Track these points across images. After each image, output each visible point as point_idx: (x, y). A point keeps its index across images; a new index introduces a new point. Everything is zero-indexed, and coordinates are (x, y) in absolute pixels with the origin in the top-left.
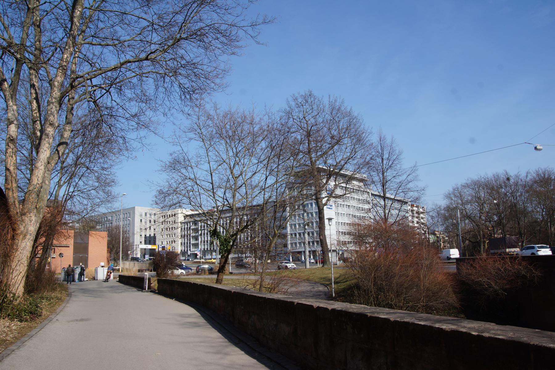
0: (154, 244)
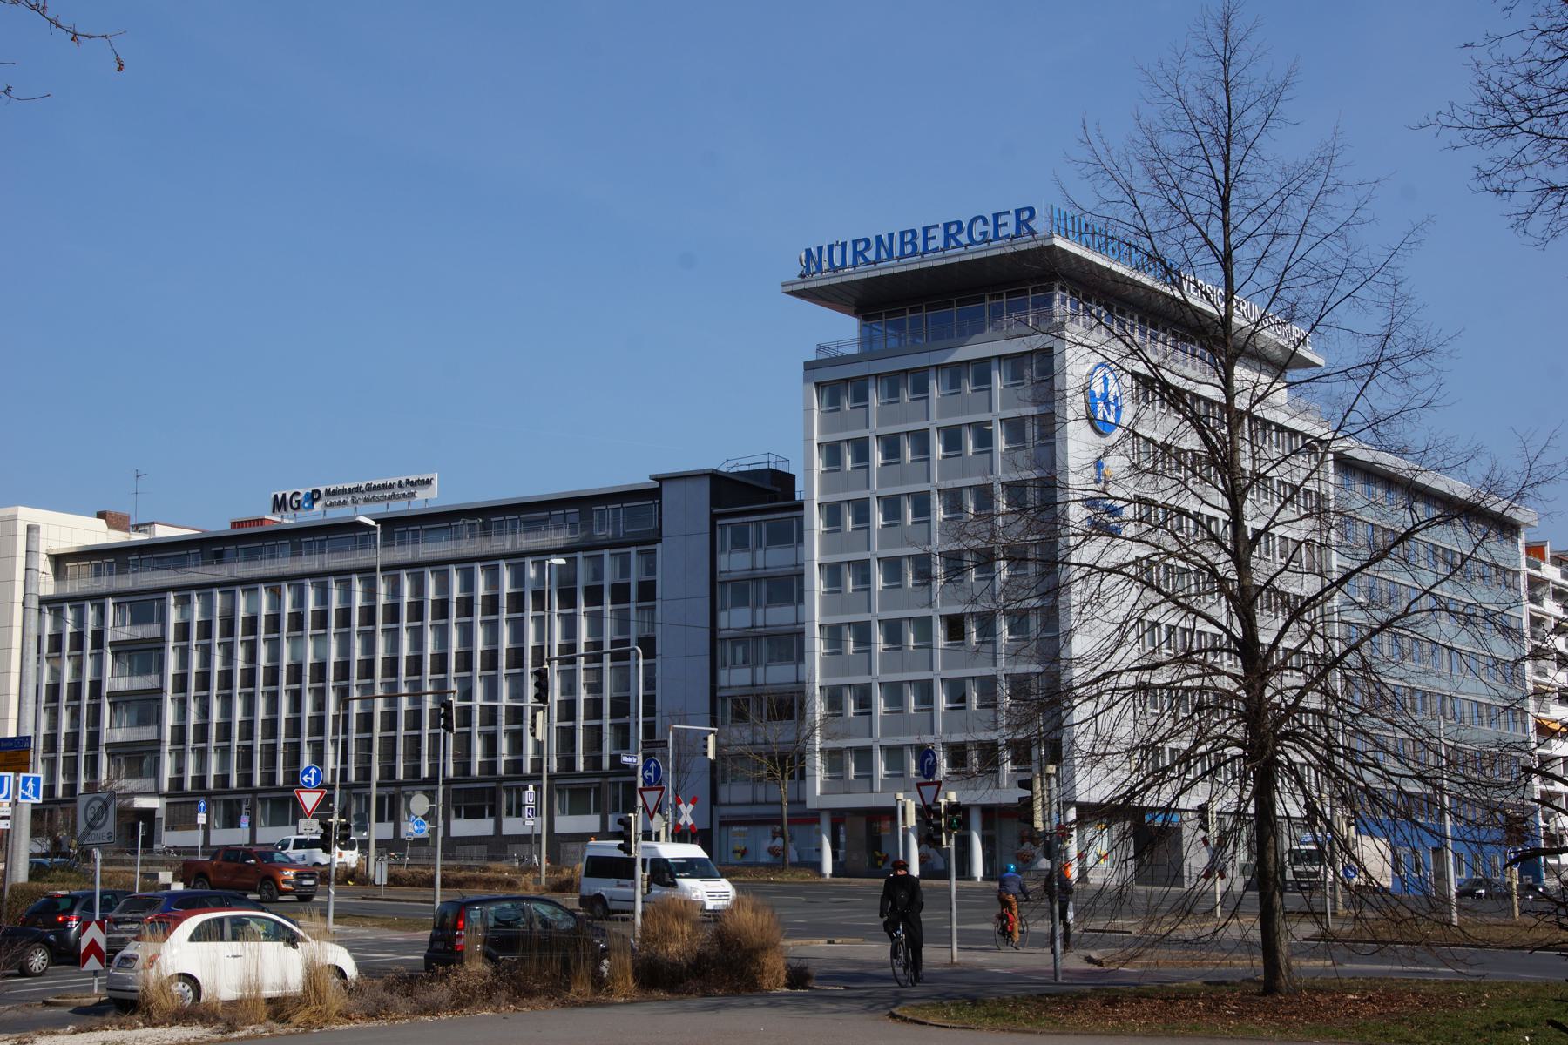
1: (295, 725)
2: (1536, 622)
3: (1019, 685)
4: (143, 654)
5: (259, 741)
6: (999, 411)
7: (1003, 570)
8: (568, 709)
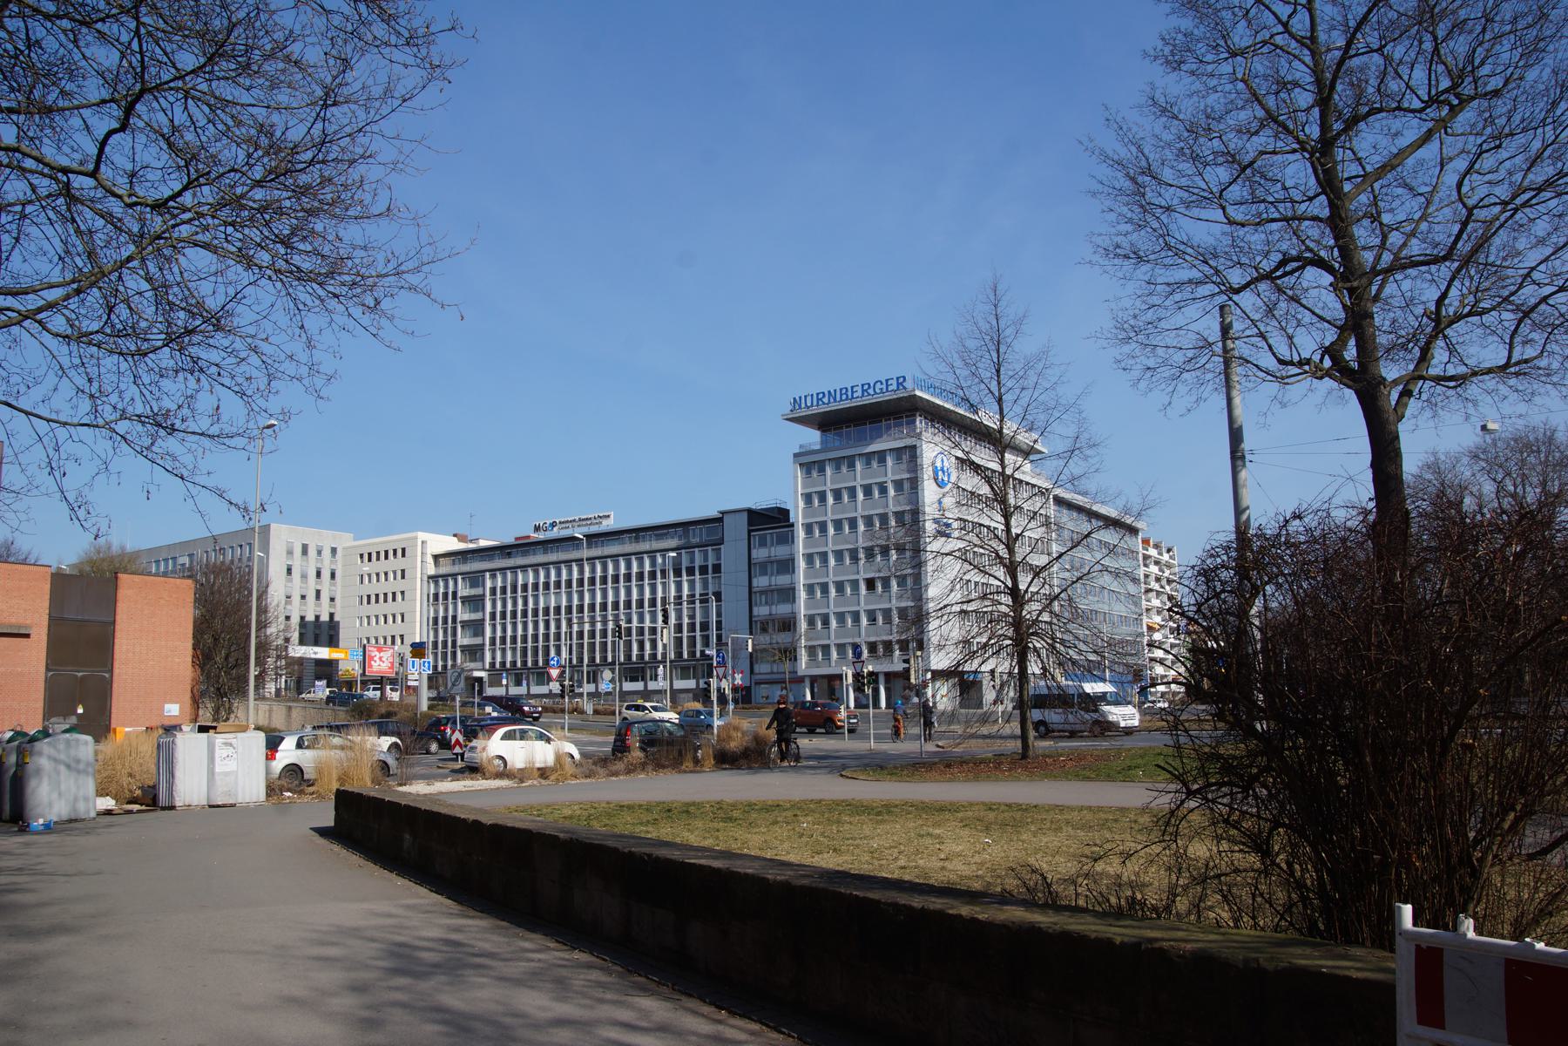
0: (333, 641)
1: (547, 636)
2: (1146, 576)
3: (903, 612)
4: (475, 602)
5: (530, 644)
6: (890, 476)
7: (894, 555)
8: (679, 628)
